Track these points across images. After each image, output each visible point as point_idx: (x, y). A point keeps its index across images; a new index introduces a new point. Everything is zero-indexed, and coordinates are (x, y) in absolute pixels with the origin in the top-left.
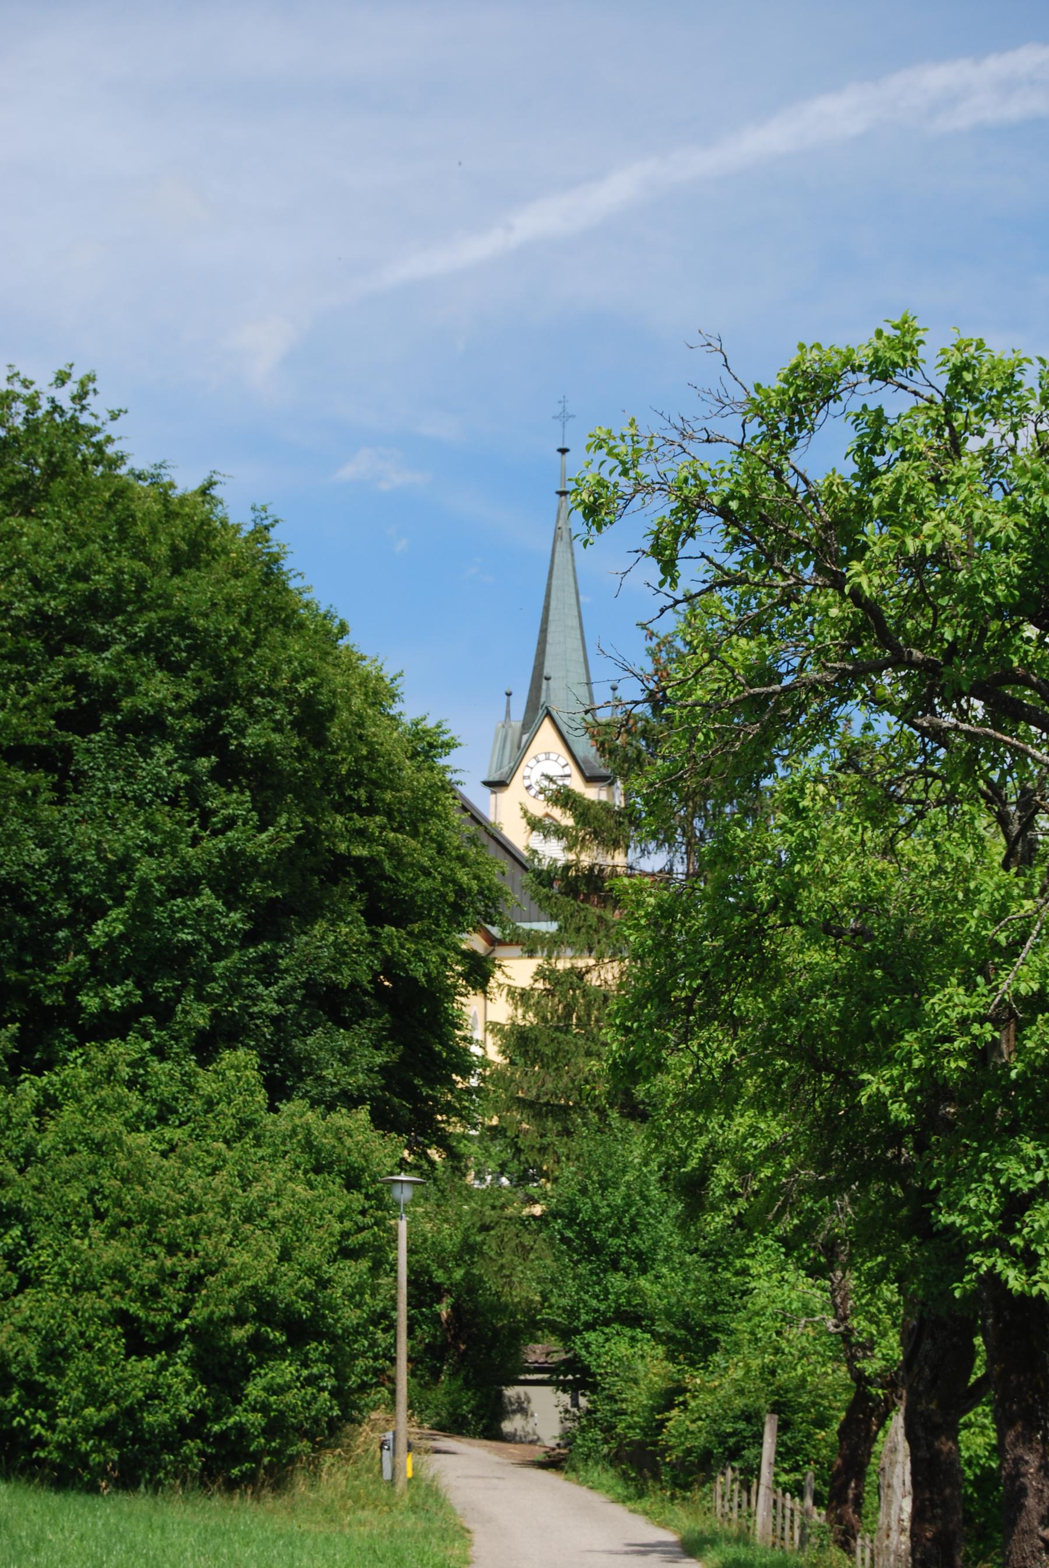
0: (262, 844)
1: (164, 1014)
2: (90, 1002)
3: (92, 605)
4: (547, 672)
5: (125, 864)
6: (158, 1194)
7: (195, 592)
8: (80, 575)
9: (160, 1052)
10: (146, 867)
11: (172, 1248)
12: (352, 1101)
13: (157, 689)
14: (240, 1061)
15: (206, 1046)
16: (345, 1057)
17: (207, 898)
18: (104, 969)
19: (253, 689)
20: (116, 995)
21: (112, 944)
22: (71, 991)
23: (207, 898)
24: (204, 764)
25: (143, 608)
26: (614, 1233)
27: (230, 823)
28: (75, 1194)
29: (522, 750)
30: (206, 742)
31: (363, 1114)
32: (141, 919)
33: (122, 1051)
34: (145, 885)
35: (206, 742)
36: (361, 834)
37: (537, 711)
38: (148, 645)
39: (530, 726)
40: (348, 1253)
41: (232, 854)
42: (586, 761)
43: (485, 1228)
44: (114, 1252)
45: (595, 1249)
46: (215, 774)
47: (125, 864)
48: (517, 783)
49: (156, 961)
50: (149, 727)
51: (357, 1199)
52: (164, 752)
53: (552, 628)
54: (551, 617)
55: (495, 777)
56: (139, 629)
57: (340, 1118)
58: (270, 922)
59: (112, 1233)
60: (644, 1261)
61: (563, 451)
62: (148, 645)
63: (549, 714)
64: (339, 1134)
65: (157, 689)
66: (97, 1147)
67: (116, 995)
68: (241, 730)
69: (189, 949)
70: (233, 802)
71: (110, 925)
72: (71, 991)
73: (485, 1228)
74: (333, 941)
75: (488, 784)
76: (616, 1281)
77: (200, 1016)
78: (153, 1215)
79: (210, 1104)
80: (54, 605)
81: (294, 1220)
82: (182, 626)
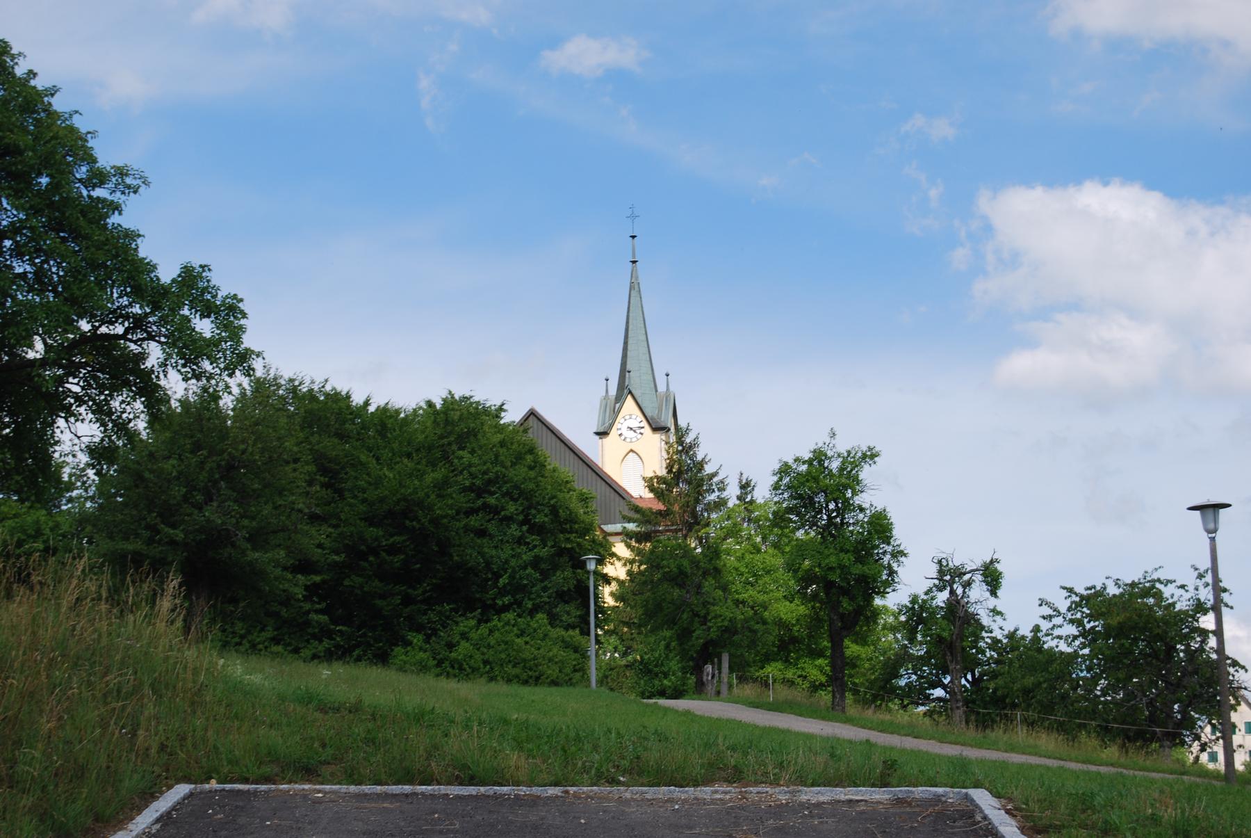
0: (544, 552)
1: (519, 604)
2: (500, 603)
3: (490, 482)
4: (629, 367)
5: (507, 562)
6: (526, 655)
7: (519, 473)
8: (485, 473)
9: (519, 616)
10: (513, 562)
11: (531, 669)
12: (574, 627)
13: (512, 508)
14: (541, 617)
15: (532, 612)
16: (568, 613)
17: (529, 570)
18: (503, 592)
19: (538, 503)
20: (506, 600)
21: (505, 586)
22: (494, 599)
23: (529, 570)
24: (525, 528)
25: (506, 483)
26: (656, 666)
27: (535, 546)
28: (503, 656)
29: (616, 413)
30: (526, 521)
31: (577, 631)
32: (512, 577)
33: (510, 616)
34: (513, 568)
35: (526, 521)
36: (568, 540)
37: (624, 390)
38: (507, 494)
39: (620, 398)
40: (575, 671)
41: (536, 557)
42: (652, 418)
43: (612, 669)
44: (517, 671)
45: (650, 671)
46: (528, 531)
47: (507, 562)
48: (614, 432)
49: (517, 588)
50: (509, 519)
51: (577, 655)
52: (514, 527)
53: (630, 342)
54: (629, 347)
55: (601, 430)
56: (504, 489)
57: (571, 632)
58: (545, 575)
59: (514, 666)
60: (666, 675)
61: (633, 237)
62: (507, 494)
63: (630, 392)
64: (571, 637)
65: (512, 508)
66: (506, 643)
67: (506, 600)
68: (535, 517)
69: (525, 586)
70: (534, 539)
71: (502, 581)
72: (494, 599)
73: (612, 669)
74: (563, 577)
75: (597, 434)
76: (656, 682)
77: (530, 605)
78: (524, 660)
79: (535, 630)
80: (478, 482)
81: (562, 662)
82: (516, 487)
